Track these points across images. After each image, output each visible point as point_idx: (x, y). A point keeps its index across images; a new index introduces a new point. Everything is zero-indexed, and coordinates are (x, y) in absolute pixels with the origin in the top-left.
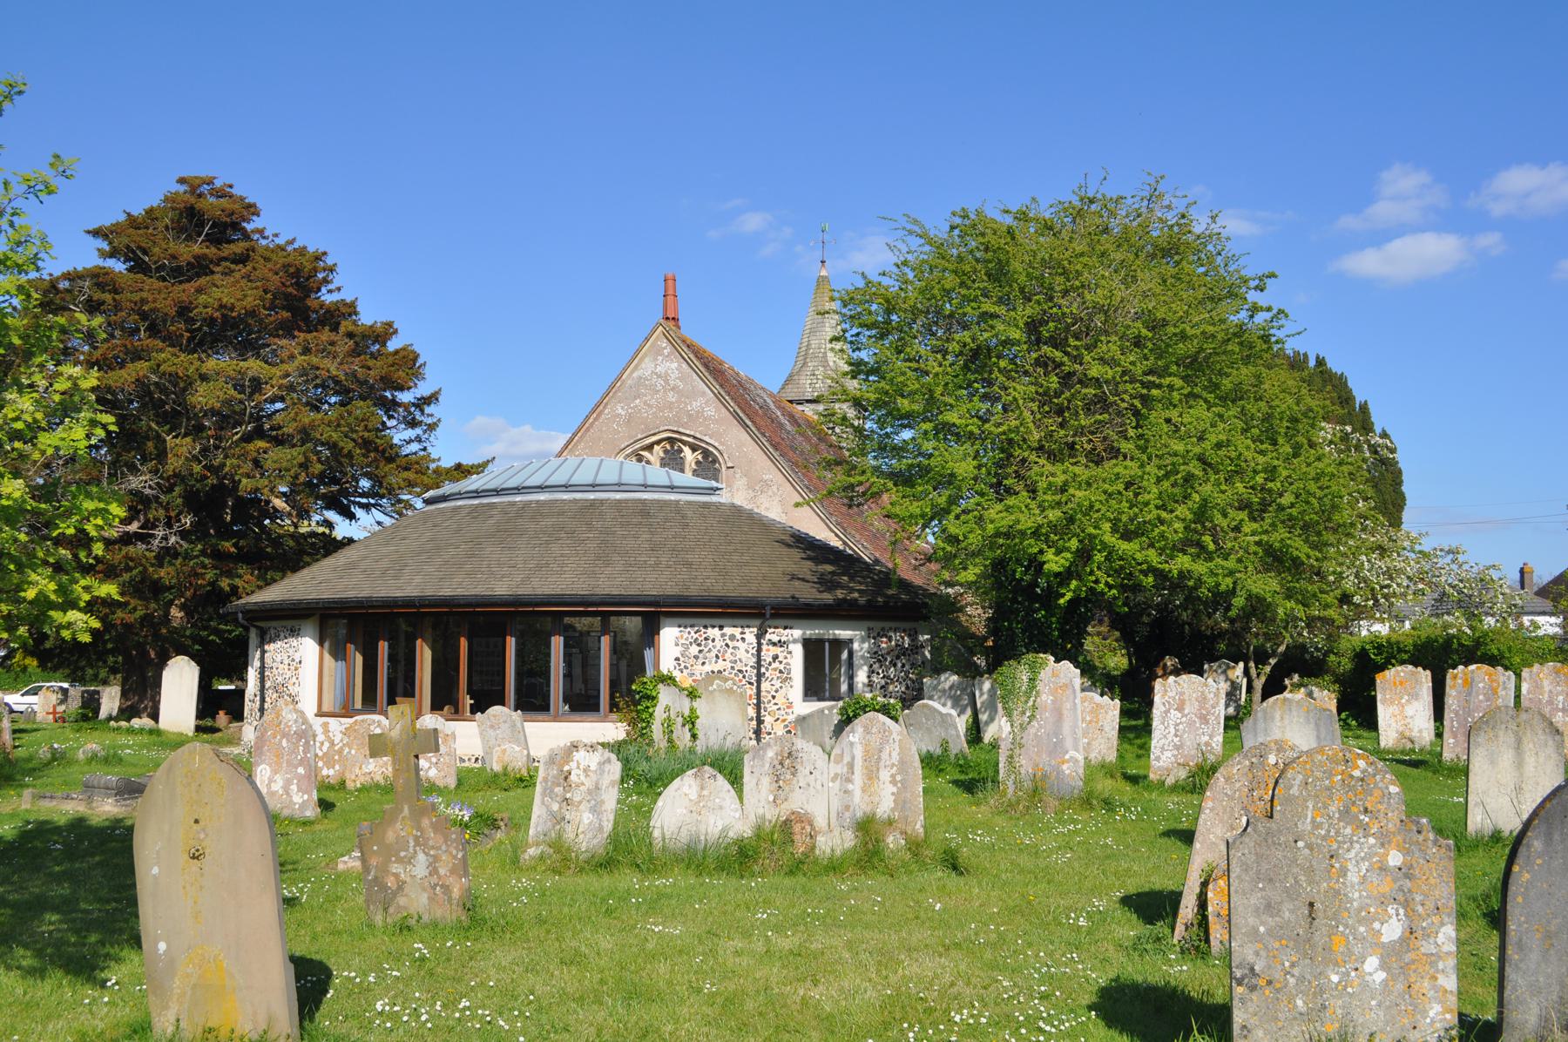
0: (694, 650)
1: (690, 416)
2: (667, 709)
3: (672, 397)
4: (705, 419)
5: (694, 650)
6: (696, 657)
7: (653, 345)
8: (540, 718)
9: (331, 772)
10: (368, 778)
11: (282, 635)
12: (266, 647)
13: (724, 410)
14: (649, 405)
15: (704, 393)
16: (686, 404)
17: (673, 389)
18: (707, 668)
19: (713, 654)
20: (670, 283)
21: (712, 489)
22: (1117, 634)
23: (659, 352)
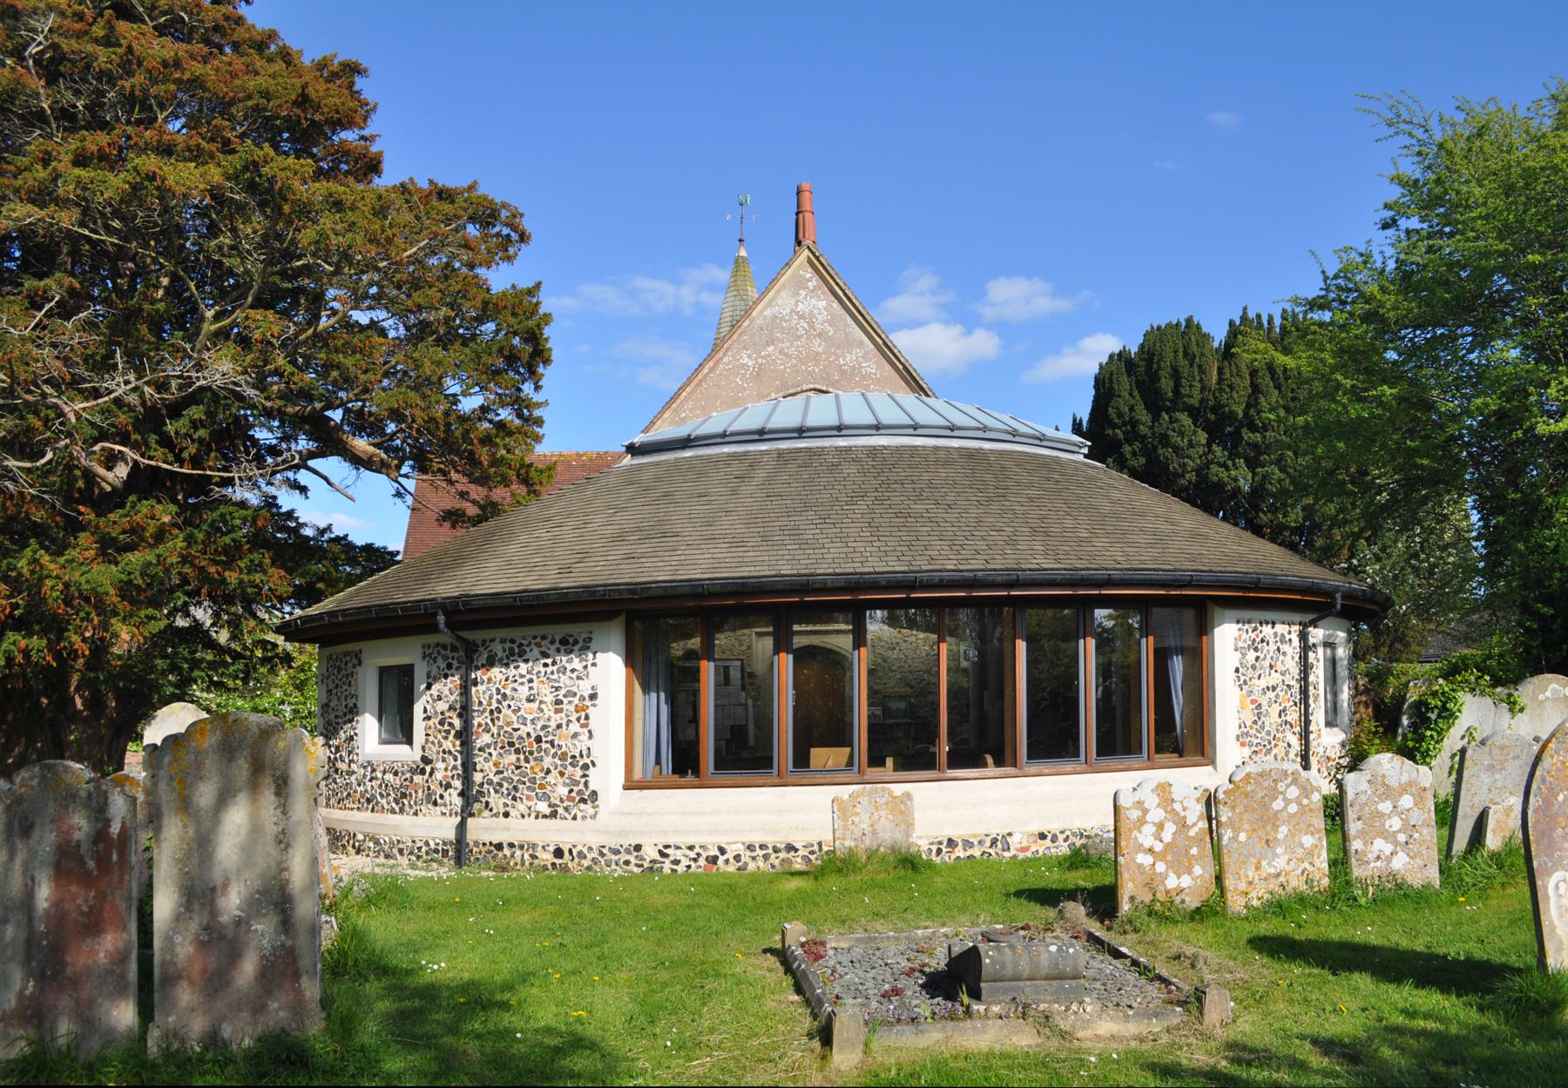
0: (1251, 655)
1: (844, 372)
2: (1469, 732)
3: (818, 346)
4: (863, 377)
5: (1251, 655)
6: (1254, 667)
7: (794, 275)
8: (1068, 768)
9: (1186, 881)
10: (1274, 885)
12: (478, 674)
13: (888, 367)
14: (787, 355)
15: (861, 343)
16: (838, 357)
17: (820, 335)
18: (1263, 683)
19: (1266, 663)
23: (800, 284)
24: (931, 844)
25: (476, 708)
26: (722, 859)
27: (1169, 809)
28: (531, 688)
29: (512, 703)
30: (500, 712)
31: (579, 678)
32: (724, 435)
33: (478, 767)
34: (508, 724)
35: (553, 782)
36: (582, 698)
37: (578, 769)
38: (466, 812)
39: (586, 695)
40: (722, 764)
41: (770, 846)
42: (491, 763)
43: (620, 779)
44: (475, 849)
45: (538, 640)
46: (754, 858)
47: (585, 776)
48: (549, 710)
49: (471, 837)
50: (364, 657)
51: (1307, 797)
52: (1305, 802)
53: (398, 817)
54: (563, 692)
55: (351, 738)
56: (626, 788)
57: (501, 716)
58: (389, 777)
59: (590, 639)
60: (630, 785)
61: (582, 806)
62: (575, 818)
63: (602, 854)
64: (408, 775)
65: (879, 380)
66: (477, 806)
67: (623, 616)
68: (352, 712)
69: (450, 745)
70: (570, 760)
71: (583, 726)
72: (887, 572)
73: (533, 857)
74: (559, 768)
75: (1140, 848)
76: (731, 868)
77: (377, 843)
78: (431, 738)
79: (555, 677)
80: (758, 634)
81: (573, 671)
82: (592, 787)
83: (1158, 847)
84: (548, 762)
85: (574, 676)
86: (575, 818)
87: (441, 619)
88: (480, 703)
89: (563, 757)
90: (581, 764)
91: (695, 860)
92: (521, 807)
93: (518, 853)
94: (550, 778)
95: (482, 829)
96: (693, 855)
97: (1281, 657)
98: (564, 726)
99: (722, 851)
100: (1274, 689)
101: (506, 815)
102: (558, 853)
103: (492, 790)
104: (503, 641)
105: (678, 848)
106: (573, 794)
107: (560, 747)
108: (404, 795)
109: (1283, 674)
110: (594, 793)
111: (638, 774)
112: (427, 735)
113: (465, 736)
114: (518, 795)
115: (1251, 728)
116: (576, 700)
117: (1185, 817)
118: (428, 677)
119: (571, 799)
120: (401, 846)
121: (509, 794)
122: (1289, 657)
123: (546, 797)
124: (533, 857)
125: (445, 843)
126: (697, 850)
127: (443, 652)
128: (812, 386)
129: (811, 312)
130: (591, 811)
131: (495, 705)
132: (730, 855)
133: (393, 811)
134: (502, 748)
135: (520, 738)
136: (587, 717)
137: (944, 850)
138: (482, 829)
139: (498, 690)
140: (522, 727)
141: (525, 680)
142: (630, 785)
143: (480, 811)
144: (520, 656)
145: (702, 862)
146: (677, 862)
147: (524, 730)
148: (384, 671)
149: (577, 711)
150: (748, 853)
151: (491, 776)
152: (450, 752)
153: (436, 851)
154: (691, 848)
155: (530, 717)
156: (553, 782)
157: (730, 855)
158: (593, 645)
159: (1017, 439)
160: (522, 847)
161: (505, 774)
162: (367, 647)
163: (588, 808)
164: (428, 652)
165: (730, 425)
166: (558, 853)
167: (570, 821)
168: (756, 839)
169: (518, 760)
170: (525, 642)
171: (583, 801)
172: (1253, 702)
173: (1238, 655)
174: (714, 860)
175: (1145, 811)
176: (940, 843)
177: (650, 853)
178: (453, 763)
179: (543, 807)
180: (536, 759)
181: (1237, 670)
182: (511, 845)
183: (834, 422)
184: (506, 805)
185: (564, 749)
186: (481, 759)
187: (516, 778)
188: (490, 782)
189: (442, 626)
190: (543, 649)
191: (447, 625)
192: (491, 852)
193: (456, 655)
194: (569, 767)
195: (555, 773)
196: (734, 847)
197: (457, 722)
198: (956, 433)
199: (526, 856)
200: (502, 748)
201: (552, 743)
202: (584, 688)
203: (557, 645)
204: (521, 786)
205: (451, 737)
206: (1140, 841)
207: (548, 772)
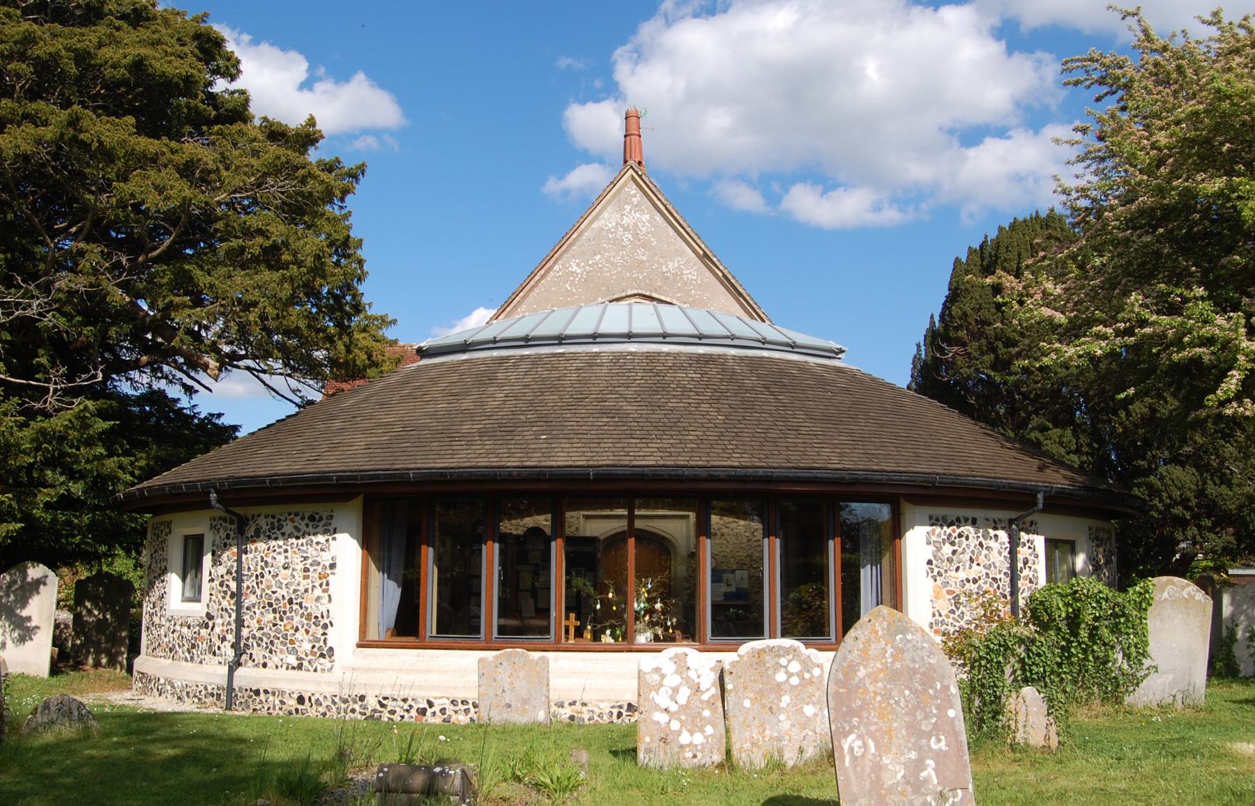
0: (947, 549)
3: (642, 255)
4: (685, 283)
5: (947, 549)
6: (950, 560)
8: (463, 642)
9: (698, 739)
11: (288, 528)
13: (708, 274)
18: (962, 575)
19: (967, 557)
20: (633, 120)
21: (831, 351)
22: (125, 578)
24: (613, 707)
25: (246, 573)
26: (429, 711)
27: (685, 676)
28: (286, 557)
29: (272, 570)
30: (263, 577)
31: (322, 550)
32: (494, 341)
33: (246, 624)
34: (268, 587)
35: (300, 638)
36: (325, 567)
37: (319, 628)
38: (235, 665)
39: (327, 564)
40: (445, 627)
41: (470, 702)
42: (255, 621)
43: (355, 637)
44: (239, 694)
45: (292, 516)
46: (456, 712)
47: (324, 634)
48: (299, 575)
49: (236, 684)
50: (173, 526)
51: (808, 671)
52: (807, 676)
53: (189, 664)
54: (310, 561)
55: (162, 597)
56: (359, 646)
57: (263, 580)
58: (185, 630)
59: (332, 517)
60: (363, 644)
61: (322, 660)
62: (315, 670)
63: (334, 702)
64: (197, 628)
65: (700, 285)
66: (244, 657)
67: (361, 497)
68: (164, 571)
69: (226, 603)
70: (313, 620)
71: (325, 591)
72: (567, 466)
73: (282, 702)
74: (305, 627)
75: (657, 708)
76: (438, 720)
77: (173, 687)
78: (214, 598)
79: (304, 548)
80: (586, 517)
81: (318, 543)
82: (330, 644)
83: (673, 708)
84: (297, 620)
85: (319, 548)
86: (315, 670)
87: (213, 496)
88: (249, 569)
89: (309, 617)
90: (322, 623)
91: (408, 711)
92: (276, 659)
93: (271, 698)
94: (299, 635)
95: (247, 676)
96: (406, 707)
97: (984, 552)
98: (310, 591)
99: (431, 704)
100: (975, 581)
101: (265, 665)
102: (301, 700)
103: (255, 644)
104: (266, 517)
105: (394, 700)
106: (315, 650)
107: (306, 608)
108: (193, 646)
109: (988, 567)
110: (331, 649)
111: (373, 635)
112: (211, 595)
113: (237, 596)
114: (274, 648)
115: (948, 617)
116: (320, 569)
117: (699, 683)
118: (213, 545)
119: (314, 654)
120: (188, 690)
121: (267, 648)
122: (995, 552)
123: (294, 651)
124: (282, 702)
125: (218, 689)
126: (410, 702)
127: (224, 524)
128: (635, 292)
129: (635, 224)
130: (329, 665)
131: (260, 571)
132: (436, 709)
133: (186, 660)
134: (263, 607)
135: (277, 599)
136: (328, 584)
137: (625, 713)
138: (247, 676)
139: (262, 558)
140: (279, 590)
141: (282, 550)
142: (363, 644)
143: (246, 662)
144: (279, 530)
145: (413, 713)
146: (393, 712)
147: (281, 592)
148: (187, 538)
149: (320, 578)
150: (452, 707)
151: (255, 632)
152: (226, 610)
153: (212, 695)
154: (405, 700)
155: (285, 582)
156: (300, 638)
157: (436, 709)
158: (334, 524)
159: (766, 346)
160: (274, 694)
161: (265, 630)
162: (174, 517)
163: (326, 662)
164: (214, 524)
165: (533, 330)
166: (301, 700)
167: (312, 673)
168: (460, 695)
169: (275, 618)
170: (282, 518)
171: (322, 655)
172: (949, 592)
173: (931, 548)
174: (422, 712)
175: (663, 676)
176: (620, 707)
177: (372, 703)
178: (228, 619)
179: (292, 660)
180: (288, 618)
181: (930, 562)
182: (266, 692)
183: (625, 331)
184: (265, 657)
185: (309, 610)
186: (248, 617)
187: (273, 634)
188: (254, 637)
189: (213, 503)
190: (296, 524)
191: (219, 501)
192: (250, 697)
193: (233, 527)
194: (313, 626)
195: (302, 631)
196: (440, 701)
197: (233, 585)
198: (703, 341)
199: (277, 702)
200: (263, 607)
201: (300, 605)
202: (326, 558)
203: (306, 521)
204: (276, 641)
205: (228, 597)
206: (657, 701)
207: (297, 630)
